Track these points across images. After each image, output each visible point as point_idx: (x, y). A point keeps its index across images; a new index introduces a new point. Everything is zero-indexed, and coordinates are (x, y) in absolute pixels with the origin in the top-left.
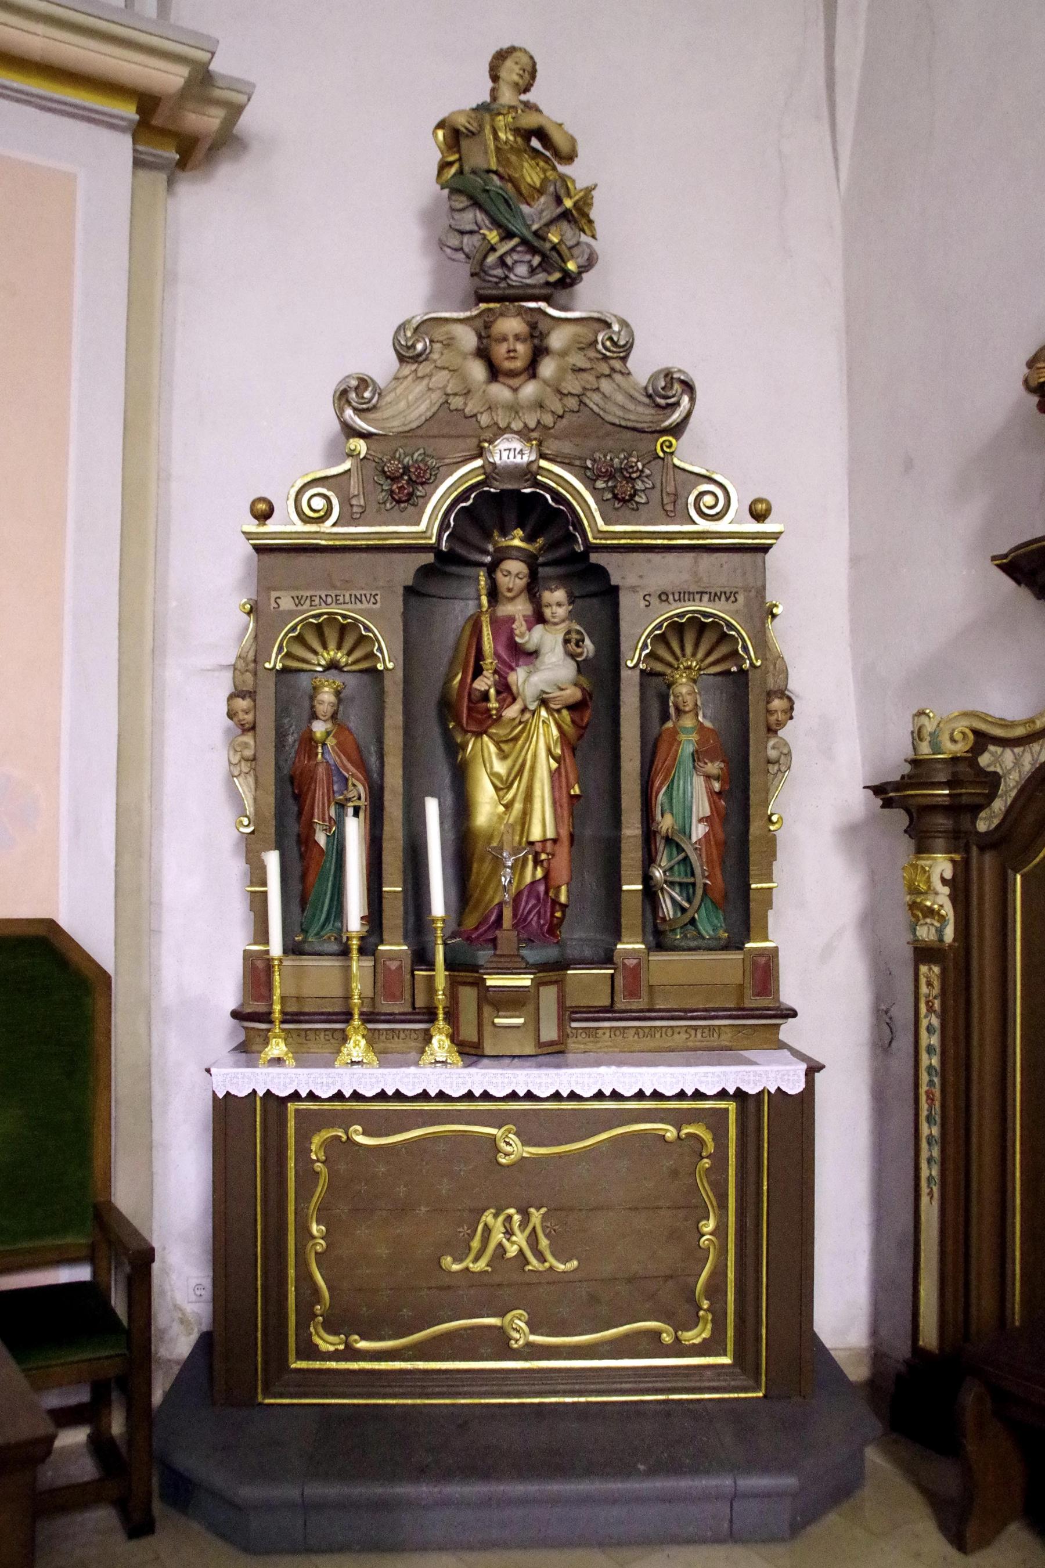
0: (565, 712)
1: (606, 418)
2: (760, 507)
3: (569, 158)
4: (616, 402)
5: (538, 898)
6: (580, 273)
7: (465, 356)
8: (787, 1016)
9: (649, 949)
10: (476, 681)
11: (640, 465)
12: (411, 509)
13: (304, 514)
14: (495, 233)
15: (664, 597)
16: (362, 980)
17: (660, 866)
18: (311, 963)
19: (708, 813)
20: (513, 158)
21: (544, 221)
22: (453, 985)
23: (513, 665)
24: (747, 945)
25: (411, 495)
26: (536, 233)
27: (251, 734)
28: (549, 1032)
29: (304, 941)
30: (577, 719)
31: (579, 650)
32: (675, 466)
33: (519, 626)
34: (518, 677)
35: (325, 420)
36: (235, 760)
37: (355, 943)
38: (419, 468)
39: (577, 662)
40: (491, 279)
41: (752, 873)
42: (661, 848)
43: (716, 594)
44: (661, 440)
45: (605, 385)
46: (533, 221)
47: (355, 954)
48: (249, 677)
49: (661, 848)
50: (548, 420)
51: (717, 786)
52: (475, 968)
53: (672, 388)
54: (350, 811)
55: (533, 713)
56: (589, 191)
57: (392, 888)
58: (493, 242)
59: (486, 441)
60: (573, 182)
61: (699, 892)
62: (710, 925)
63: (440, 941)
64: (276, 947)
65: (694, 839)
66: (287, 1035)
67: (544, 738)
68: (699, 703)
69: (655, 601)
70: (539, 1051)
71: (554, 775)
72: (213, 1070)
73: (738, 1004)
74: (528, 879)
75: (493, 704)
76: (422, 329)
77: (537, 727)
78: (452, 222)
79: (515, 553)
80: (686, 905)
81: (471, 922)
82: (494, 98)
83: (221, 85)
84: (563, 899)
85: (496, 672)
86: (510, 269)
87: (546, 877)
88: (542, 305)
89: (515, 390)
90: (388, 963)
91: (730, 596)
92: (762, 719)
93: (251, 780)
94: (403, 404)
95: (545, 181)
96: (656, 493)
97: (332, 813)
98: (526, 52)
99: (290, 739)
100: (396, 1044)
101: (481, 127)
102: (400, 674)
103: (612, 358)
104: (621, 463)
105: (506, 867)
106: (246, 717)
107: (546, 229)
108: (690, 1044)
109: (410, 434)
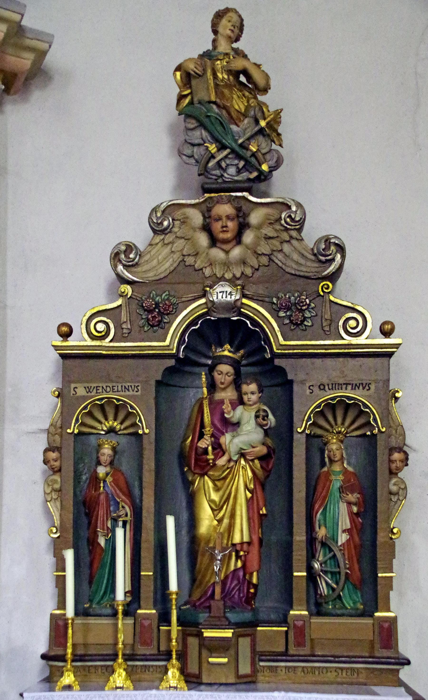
0: (257, 462)
1: (286, 270)
2: (387, 327)
3: (265, 90)
4: (293, 258)
5: (238, 580)
6: (271, 172)
8: (403, 664)
9: (311, 614)
10: (199, 442)
11: (307, 301)
12: (160, 331)
13: (95, 336)
14: (214, 146)
15: (322, 387)
16: (124, 632)
17: (318, 560)
18: (93, 622)
19: (349, 526)
21: (248, 135)
22: (184, 637)
23: (224, 431)
24: (377, 614)
25: (160, 322)
26: (241, 146)
27: (58, 474)
28: (245, 668)
29: (90, 607)
30: (264, 465)
31: (265, 422)
32: (331, 301)
33: (227, 407)
34: (226, 439)
35: (106, 272)
36: (48, 491)
37: (120, 608)
38: (166, 304)
39: (264, 429)
40: (211, 176)
41: (379, 566)
42: (319, 549)
43: (356, 385)
44: (322, 284)
45: (286, 248)
47: (120, 616)
48: (57, 438)
49: (319, 549)
50: (248, 271)
51: (355, 509)
52: (196, 624)
53: (330, 248)
54: (121, 524)
55: (236, 462)
56: (278, 113)
57: (147, 573)
58: (213, 152)
59: (207, 286)
60: (267, 107)
61: (343, 578)
62: (351, 600)
63: (174, 607)
64: (70, 612)
65: (340, 543)
66: (76, 671)
67: (243, 477)
68: (344, 455)
69: (316, 390)
70: (238, 681)
71: (249, 501)
72: (25, 695)
73: (371, 653)
74: (232, 568)
75: (211, 456)
76: (167, 211)
77: (238, 471)
78: (187, 138)
79: (225, 360)
80: (335, 586)
81: (197, 595)
82: (215, 47)
83: (30, 36)
84: (255, 581)
85: (212, 436)
86: (225, 170)
87: (244, 566)
88: (245, 194)
89: (227, 252)
90: (144, 621)
91: (366, 386)
92: (386, 465)
93: (58, 504)
94: (155, 262)
95: (248, 108)
96: (318, 319)
97: (109, 525)
98: (236, 12)
99: (84, 478)
100: (146, 676)
101: (205, 70)
102: (153, 436)
103: (291, 230)
104: (296, 299)
105: (217, 560)
106: (55, 463)
107: (247, 142)
108: (339, 680)
109: (159, 282)
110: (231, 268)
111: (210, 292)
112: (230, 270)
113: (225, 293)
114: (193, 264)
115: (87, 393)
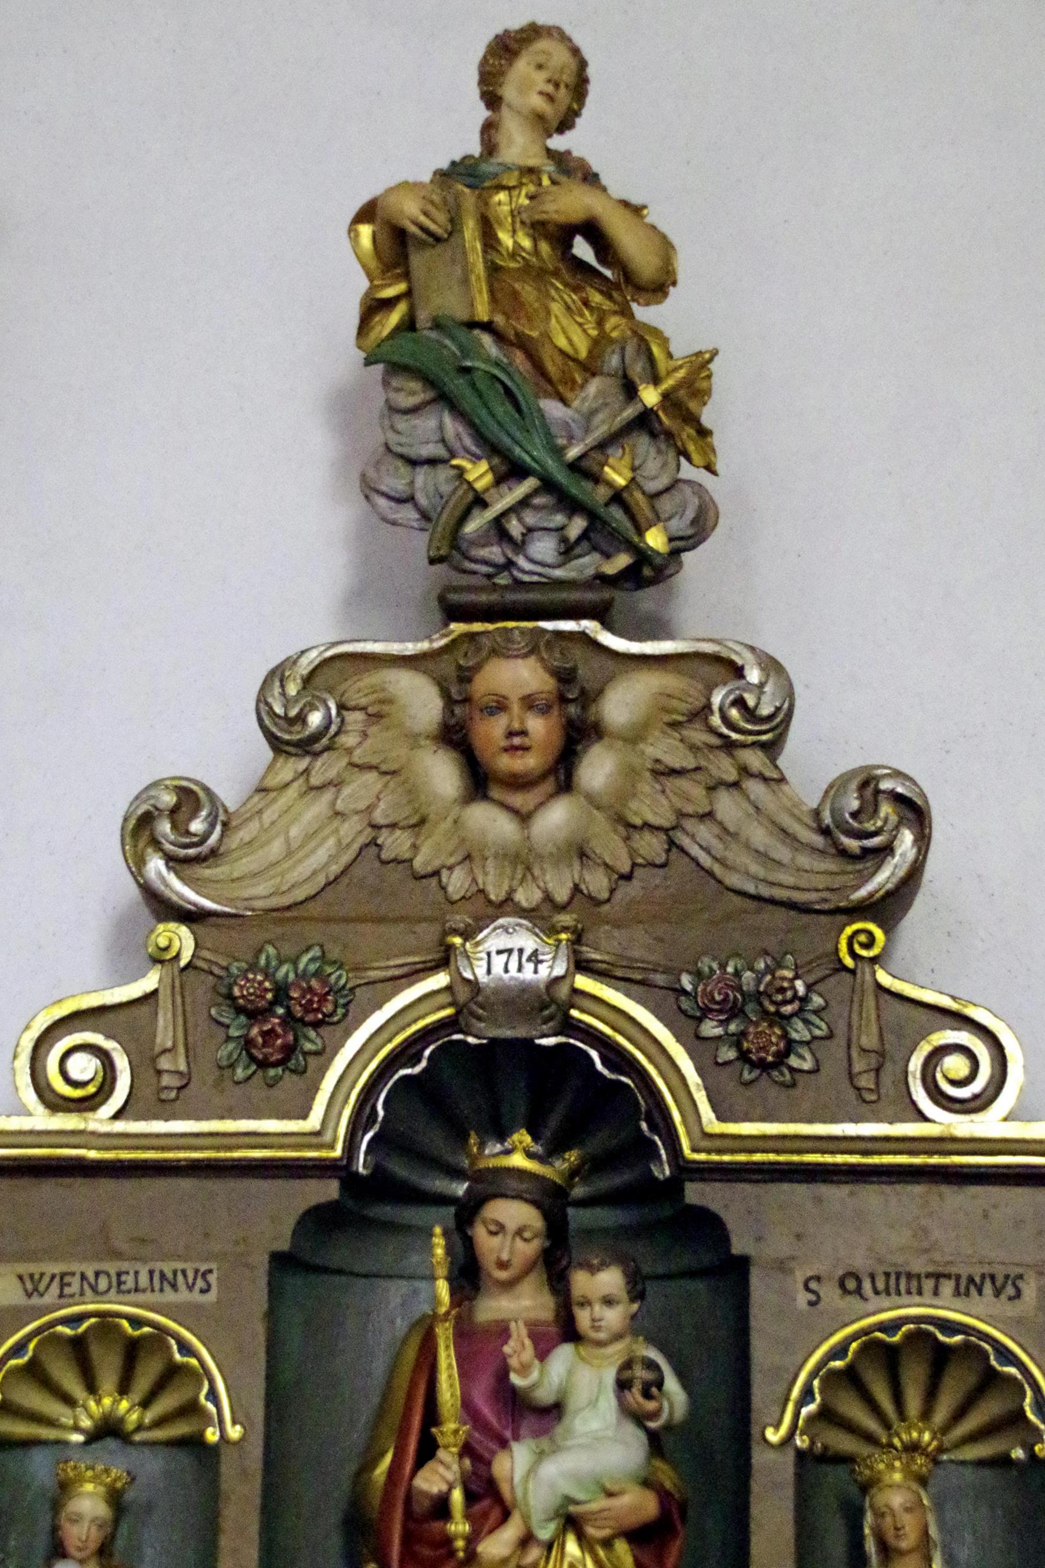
3: (659, 288)
6: (675, 554)
7: (413, 739)
14: (483, 466)
20: (528, 291)
26: (575, 467)
46: (571, 438)
50: (597, 883)
58: (479, 486)
59: (455, 932)
60: (664, 342)
78: (393, 438)
82: (490, 148)
86: (519, 547)
89: (524, 818)
101: (455, 224)
110: (537, 872)
111: (465, 950)
112: (534, 878)
113: (515, 956)
114: (407, 856)
115: (29, 1295)
